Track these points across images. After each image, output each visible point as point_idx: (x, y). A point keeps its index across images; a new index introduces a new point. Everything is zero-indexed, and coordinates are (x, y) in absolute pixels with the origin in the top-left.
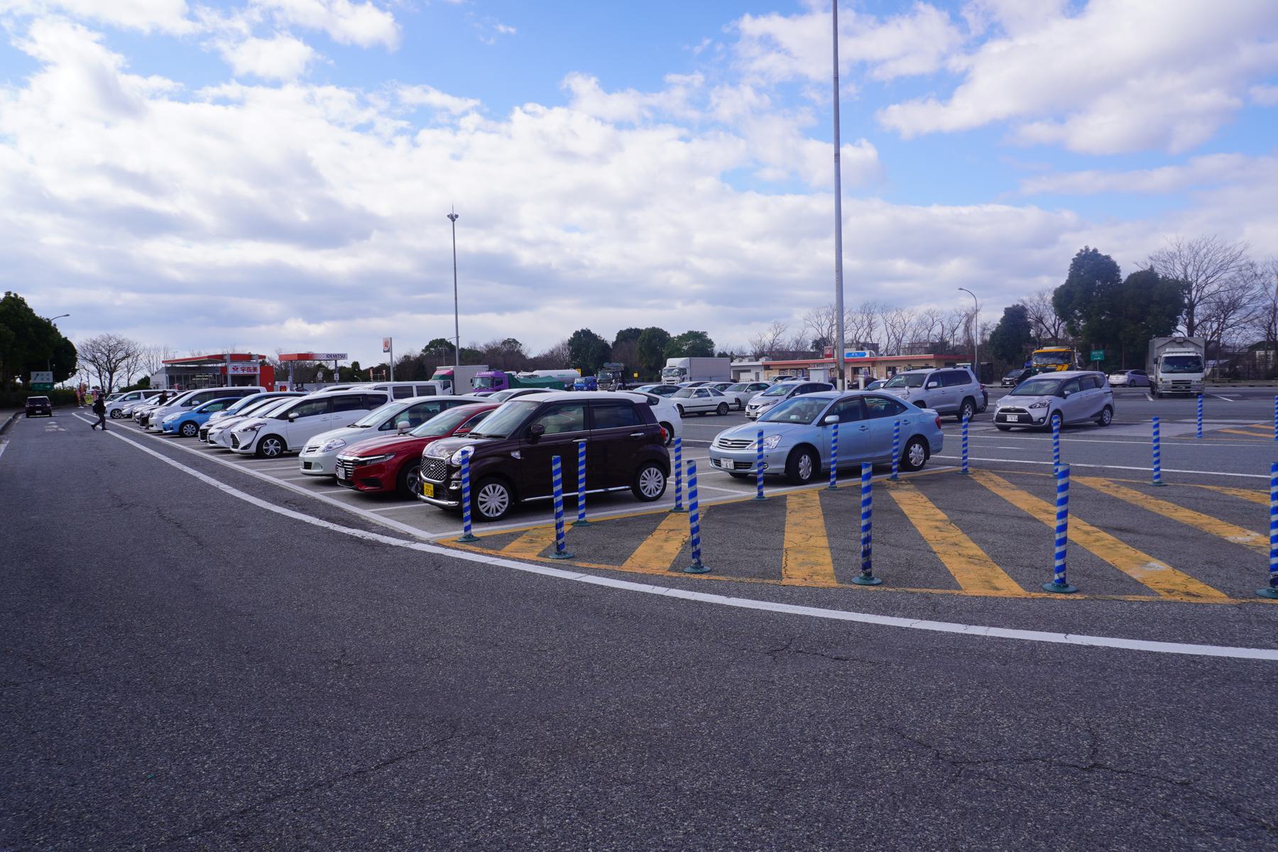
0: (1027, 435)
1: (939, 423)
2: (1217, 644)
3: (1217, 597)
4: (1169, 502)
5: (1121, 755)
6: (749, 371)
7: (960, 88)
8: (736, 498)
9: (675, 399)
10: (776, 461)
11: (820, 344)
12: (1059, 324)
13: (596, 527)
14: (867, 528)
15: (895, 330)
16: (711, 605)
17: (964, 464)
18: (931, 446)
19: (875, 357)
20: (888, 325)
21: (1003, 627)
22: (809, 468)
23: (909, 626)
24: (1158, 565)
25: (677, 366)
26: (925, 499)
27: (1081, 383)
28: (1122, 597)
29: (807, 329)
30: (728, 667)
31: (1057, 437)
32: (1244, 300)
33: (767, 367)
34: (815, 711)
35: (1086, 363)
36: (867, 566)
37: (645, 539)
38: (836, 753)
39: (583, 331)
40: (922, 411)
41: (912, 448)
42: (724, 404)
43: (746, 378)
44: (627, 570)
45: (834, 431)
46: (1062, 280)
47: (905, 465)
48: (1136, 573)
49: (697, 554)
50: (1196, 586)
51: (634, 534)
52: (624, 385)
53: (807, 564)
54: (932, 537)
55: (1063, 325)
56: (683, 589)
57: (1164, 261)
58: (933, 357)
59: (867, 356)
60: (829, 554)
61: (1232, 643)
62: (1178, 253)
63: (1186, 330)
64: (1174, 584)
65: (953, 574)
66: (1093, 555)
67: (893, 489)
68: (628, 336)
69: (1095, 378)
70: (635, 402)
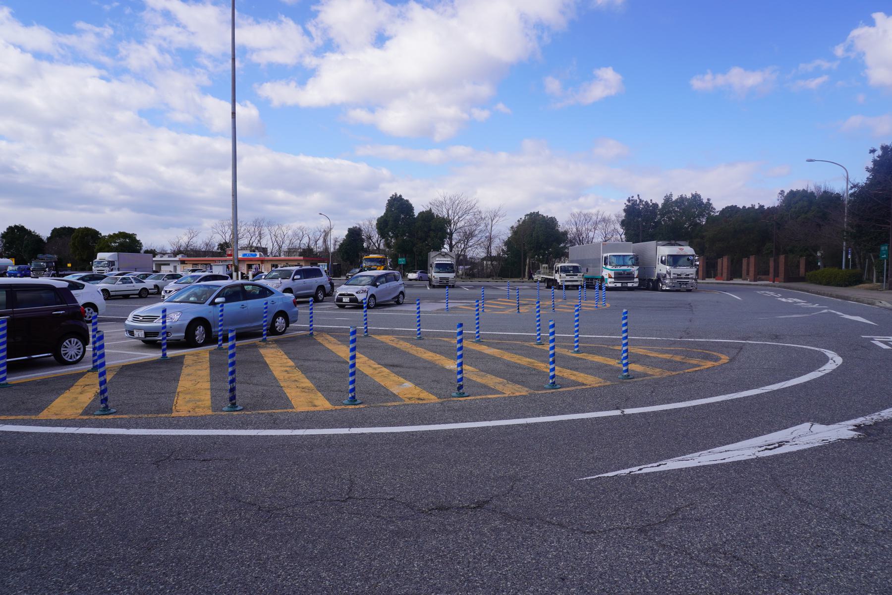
0: (355, 310)
1: (296, 303)
2: (426, 424)
3: (433, 399)
4: (422, 348)
5: (363, 490)
6: (169, 264)
7: (311, 80)
8: (145, 359)
9: (102, 285)
10: (178, 331)
11: (224, 246)
12: (380, 241)
13: (18, 387)
14: (232, 373)
15: (277, 239)
16: (114, 436)
17: (311, 329)
18: (290, 318)
19: (263, 257)
20: (272, 235)
21: (314, 428)
22: (203, 335)
23: (256, 434)
24: (408, 385)
25: (107, 259)
26: (283, 353)
27: (386, 278)
28: (385, 404)
29: (214, 235)
30: (120, 477)
31: (366, 311)
32: (477, 232)
33: (183, 262)
34: (181, 496)
35: (395, 266)
36: (233, 398)
37: (62, 393)
38: (192, 519)
39: (16, 226)
40: (284, 295)
41: (277, 320)
42: (145, 289)
43: (166, 270)
44: (42, 418)
45: (220, 309)
46: (382, 212)
47: (273, 331)
48: (395, 390)
49: (105, 400)
50: (424, 394)
51: (53, 390)
52: (57, 273)
53: (192, 401)
54: (282, 377)
55: (383, 241)
56: (91, 427)
57: (437, 206)
58: (302, 259)
59: (258, 256)
60: (210, 393)
61: (434, 423)
62: (444, 202)
63: (449, 247)
64: (414, 394)
65: (290, 399)
66: (375, 382)
67: (263, 347)
68: (61, 234)
69: (394, 275)
70: (57, 287)
